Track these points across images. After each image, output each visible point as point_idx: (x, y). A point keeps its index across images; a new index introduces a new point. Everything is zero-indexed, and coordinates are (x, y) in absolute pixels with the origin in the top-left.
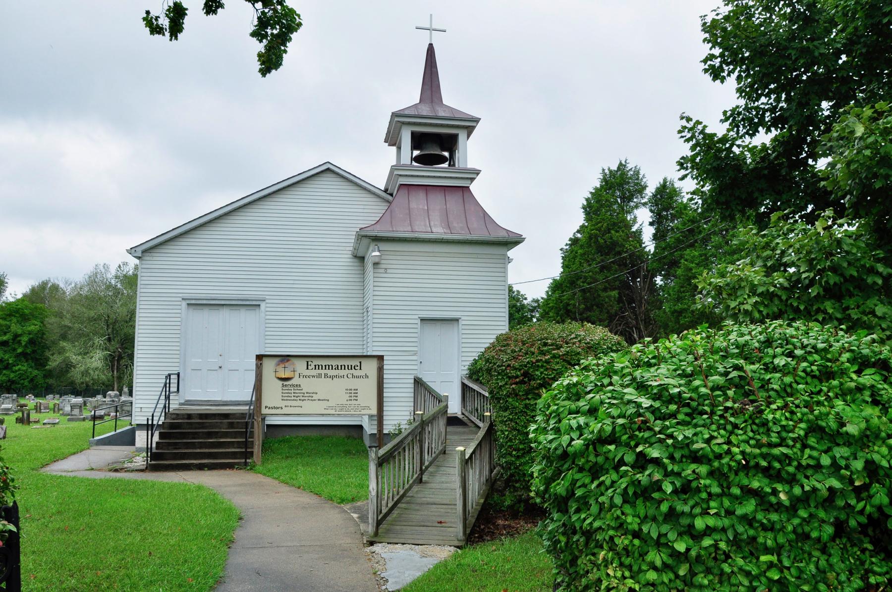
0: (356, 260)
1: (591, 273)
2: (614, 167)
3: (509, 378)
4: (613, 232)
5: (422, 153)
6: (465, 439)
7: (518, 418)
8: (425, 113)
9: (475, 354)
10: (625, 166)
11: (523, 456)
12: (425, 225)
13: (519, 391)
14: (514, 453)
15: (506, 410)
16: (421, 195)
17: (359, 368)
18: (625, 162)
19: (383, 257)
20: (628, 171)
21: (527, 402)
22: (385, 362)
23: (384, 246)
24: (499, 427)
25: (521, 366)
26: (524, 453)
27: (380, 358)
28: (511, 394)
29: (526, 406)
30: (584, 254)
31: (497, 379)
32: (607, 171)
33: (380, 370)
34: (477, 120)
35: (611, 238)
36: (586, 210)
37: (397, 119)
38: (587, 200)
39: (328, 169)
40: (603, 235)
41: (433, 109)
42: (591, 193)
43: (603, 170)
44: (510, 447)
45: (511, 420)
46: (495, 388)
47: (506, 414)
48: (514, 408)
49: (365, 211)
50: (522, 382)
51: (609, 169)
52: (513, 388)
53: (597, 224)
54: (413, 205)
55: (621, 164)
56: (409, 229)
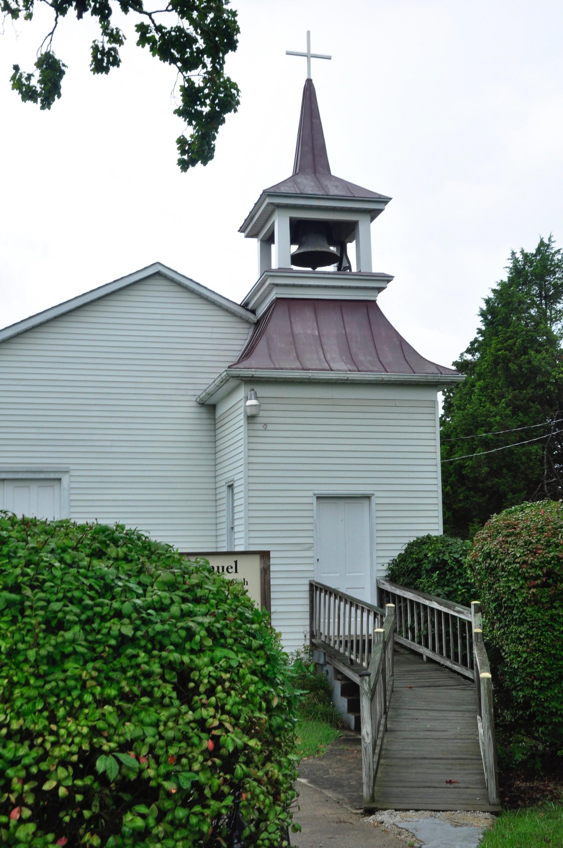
0: (202, 410)
1: (498, 418)
2: (531, 249)
3: (525, 579)
4: (532, 353)
5: (302, 250)
6: (410, 671)
7: (542, 635)
8: (309, 190)
9: (399, 547)
10: (548, 246)
11: (549, 687)
12: (319, 360)
13: (541, 597)
14: (536, 683)
15: (521, 624)
16: (309, 313)
17: (234, 569)
18: (549, 239)
19: (263, 407)
20: (554, 255)
21: (554, 611)
22: (272, 561)
23: (264, 391)
24: (508, 648)
25: (541, 562)
26: (550, 683)
27: (265, 555)
28: (529, 601)
29: (552, 618)
30: (486, 388)
31: (508, 581)
32: (519, 256)
33: (265, 572)
34: (385, 201)
35: (529, 362)
36: (486, 318)
37: (268, 200)
38: (488, 301)
39: (158, 274)
40: (516, 357)
41: (320, 185)
42: (494, 291)
43: (513, 253)
44: (530, 675)
45: (531, 637)
46: (504, 593)
47: (523, 629)
48: (535, 620)
49: (214, 336)
50: (545, 585)
51: (522, 252)
52: (533, 593)
53: (506, 340)
54: (298, 329)
55: (542, 243)
56: (298, 365)
